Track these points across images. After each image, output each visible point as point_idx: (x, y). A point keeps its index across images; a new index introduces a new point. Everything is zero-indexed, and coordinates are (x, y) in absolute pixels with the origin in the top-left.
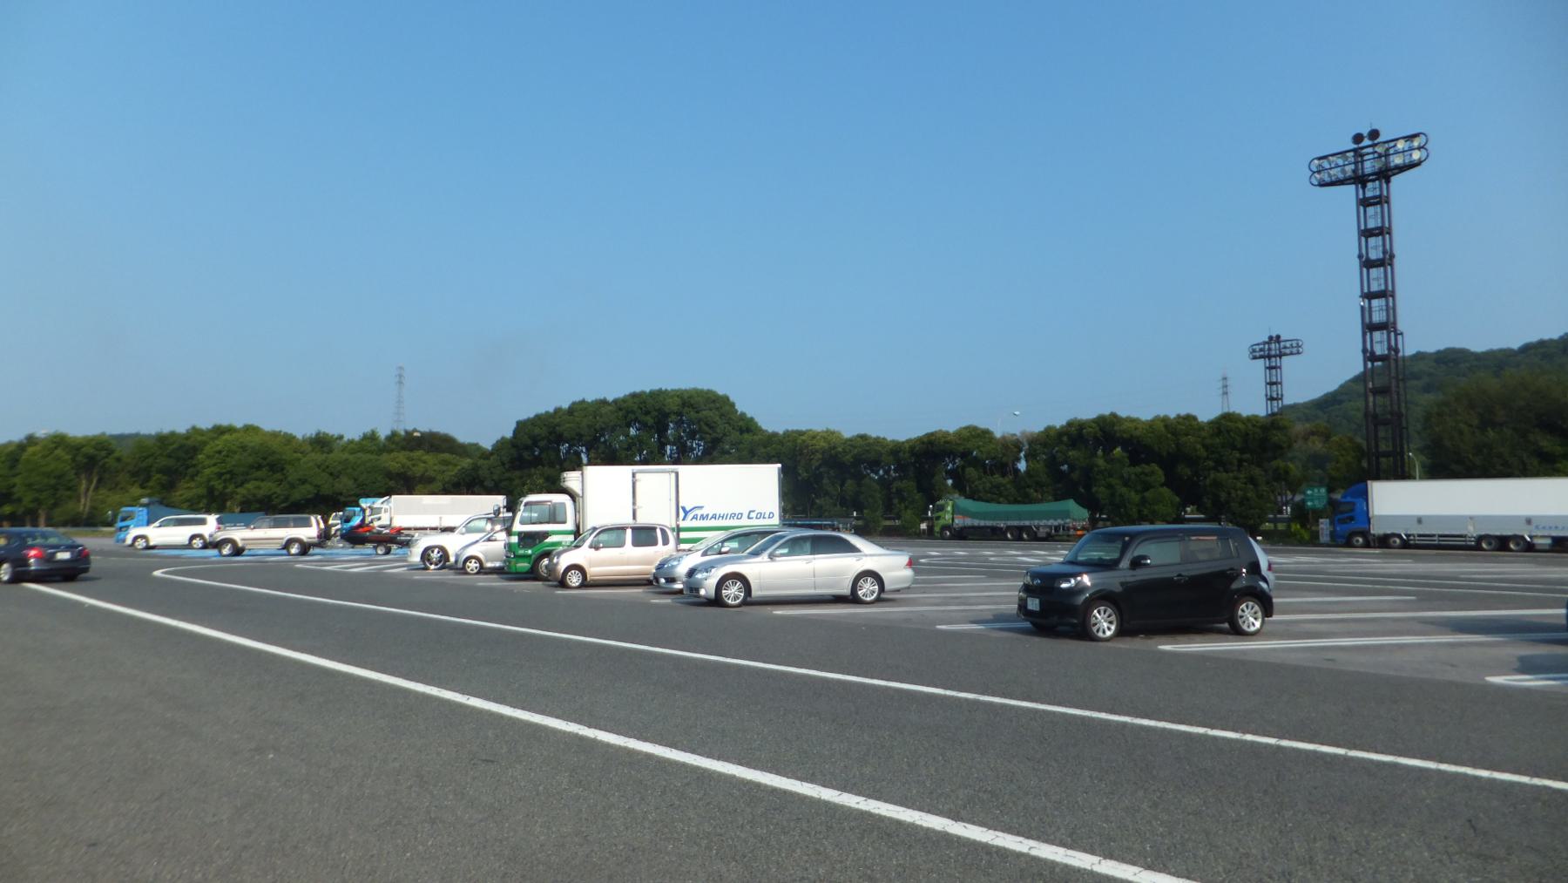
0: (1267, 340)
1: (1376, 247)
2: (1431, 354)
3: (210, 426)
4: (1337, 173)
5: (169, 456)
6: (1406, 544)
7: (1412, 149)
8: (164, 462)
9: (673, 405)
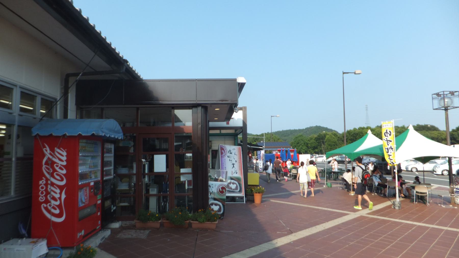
5: (351, 136)
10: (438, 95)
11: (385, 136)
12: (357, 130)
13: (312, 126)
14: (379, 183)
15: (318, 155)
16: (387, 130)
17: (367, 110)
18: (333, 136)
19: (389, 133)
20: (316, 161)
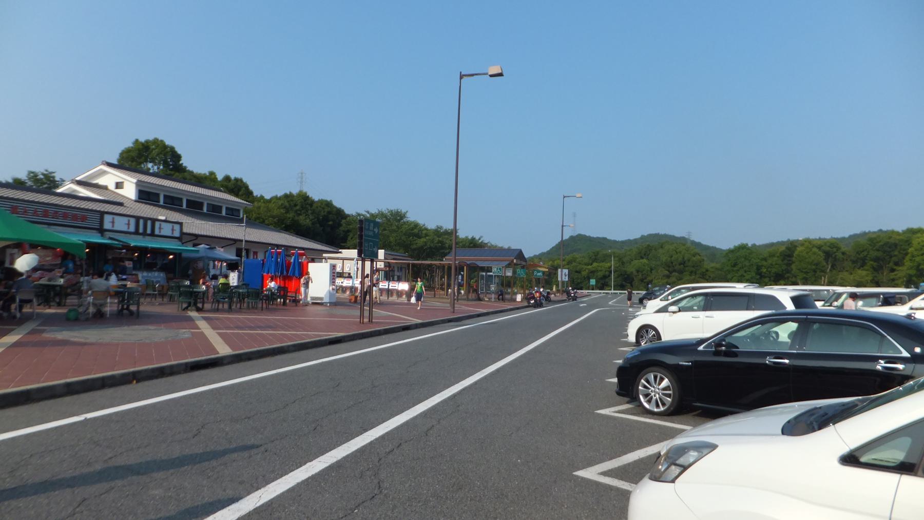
3: (905, 228)
5: (878, 250)
8: (874, 254)
13: (867, 231)
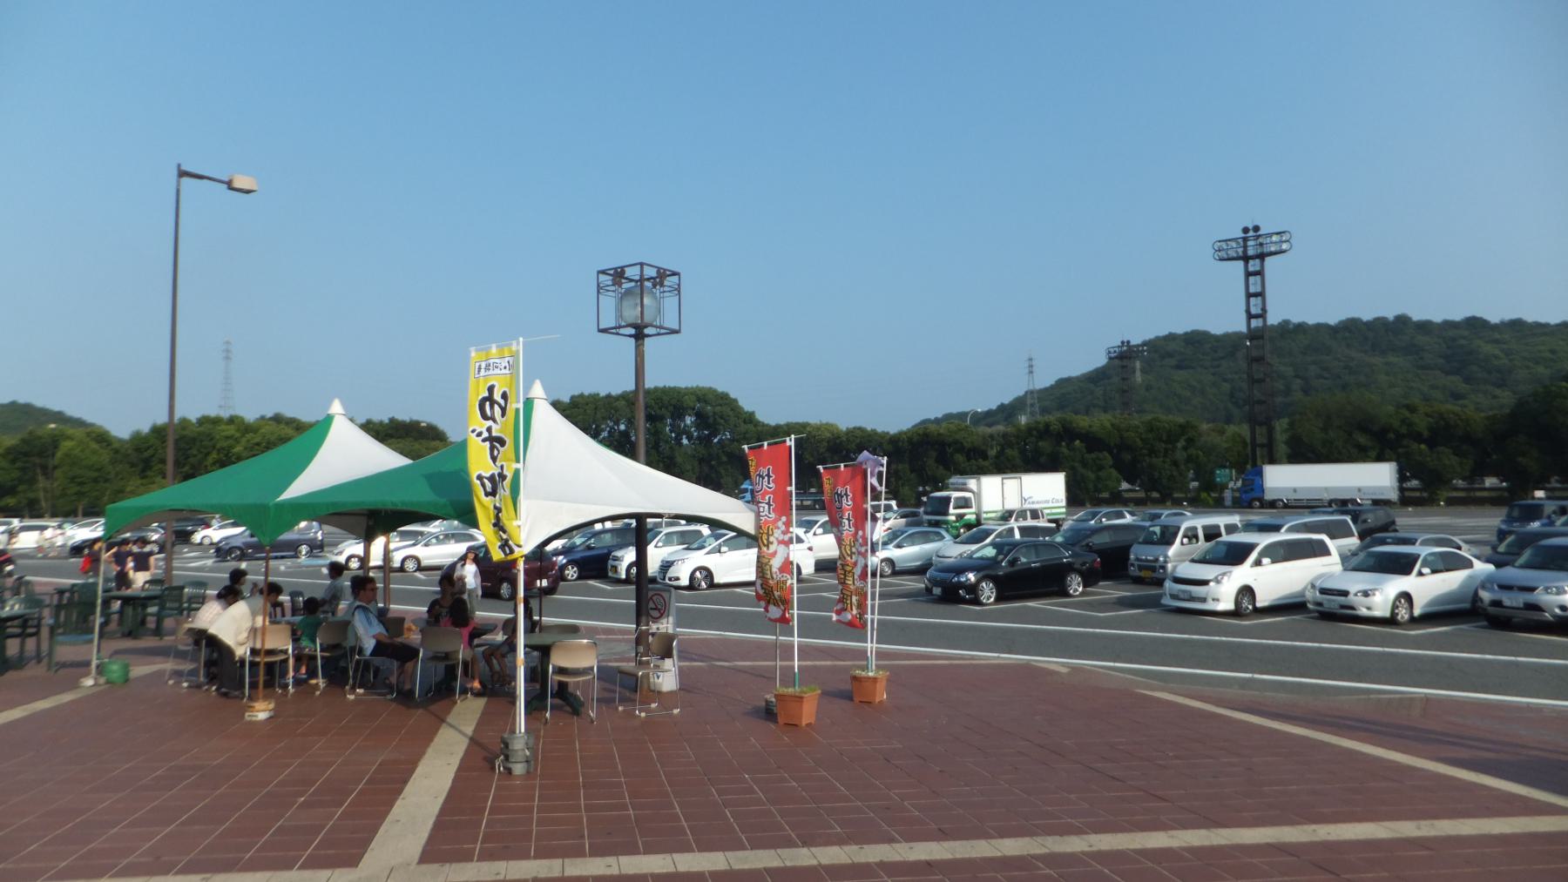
0: (1120, 344)
1: (1255, 305)
2: (1180, 335)
4: (1232, 254)
6: (1286, 506)
7: (1282, 242)
9: (689, 401)
10: (618, 275)
11: (485, 417)
12: (193, 424)
14: (381, 638)
15: (21, 522)
16: (491, 389)
17: (227, 358)
18: (94, 446)
19: (502, 402)
20: (10, 547)
